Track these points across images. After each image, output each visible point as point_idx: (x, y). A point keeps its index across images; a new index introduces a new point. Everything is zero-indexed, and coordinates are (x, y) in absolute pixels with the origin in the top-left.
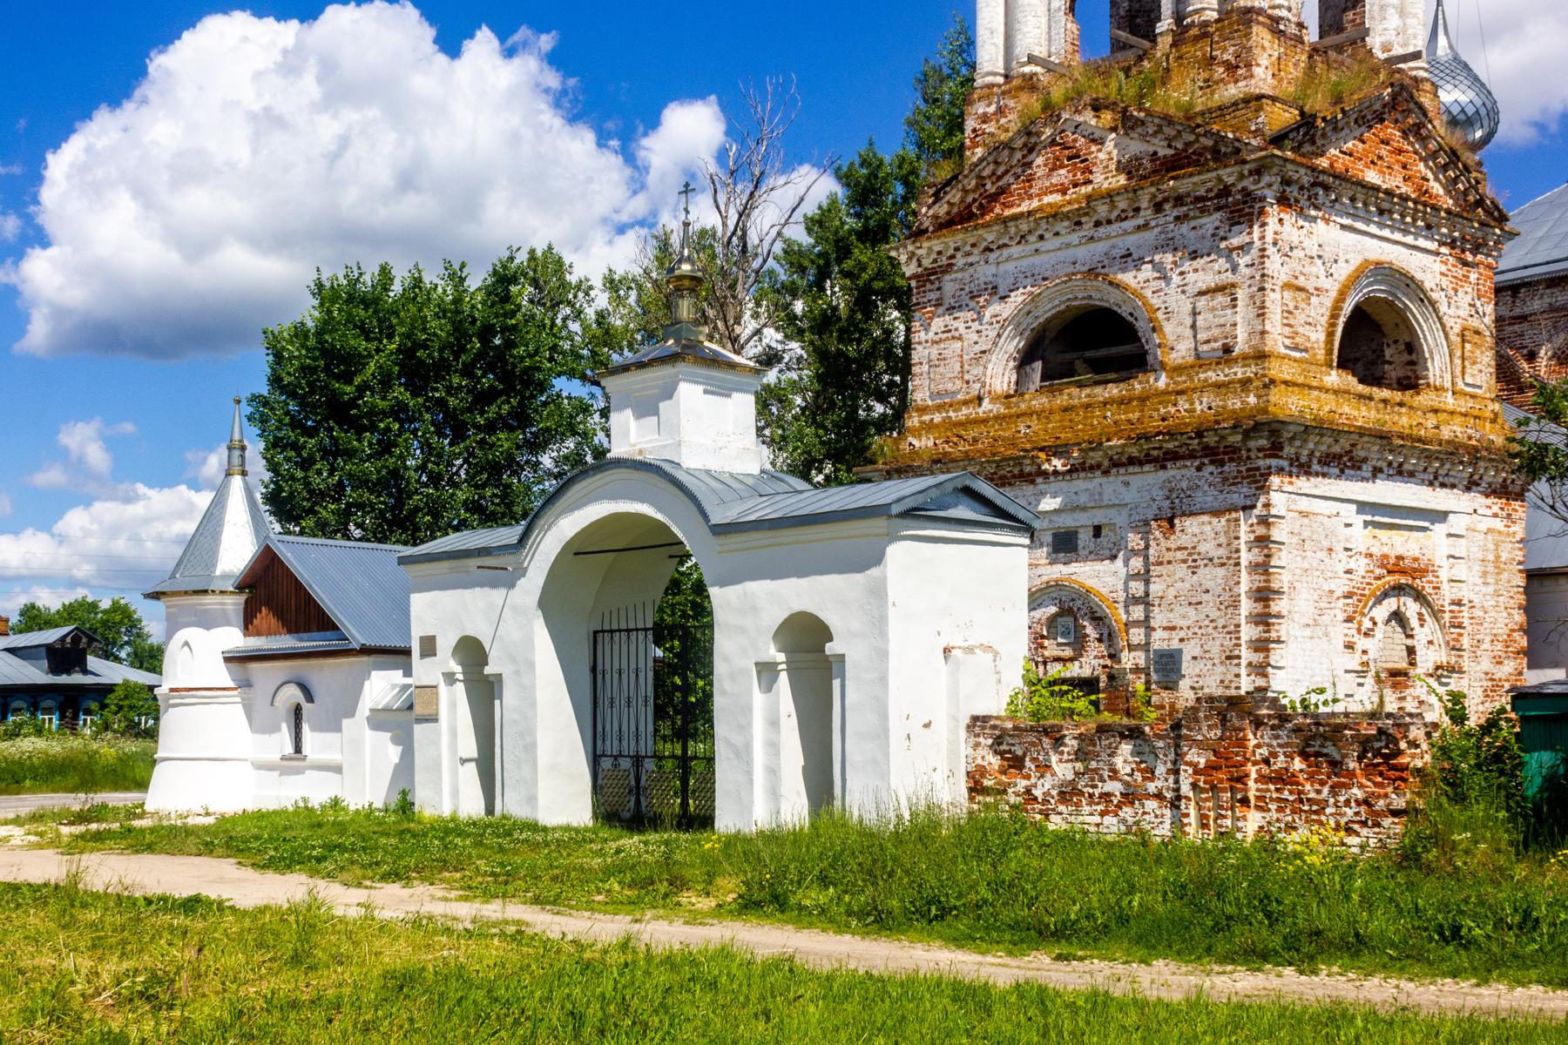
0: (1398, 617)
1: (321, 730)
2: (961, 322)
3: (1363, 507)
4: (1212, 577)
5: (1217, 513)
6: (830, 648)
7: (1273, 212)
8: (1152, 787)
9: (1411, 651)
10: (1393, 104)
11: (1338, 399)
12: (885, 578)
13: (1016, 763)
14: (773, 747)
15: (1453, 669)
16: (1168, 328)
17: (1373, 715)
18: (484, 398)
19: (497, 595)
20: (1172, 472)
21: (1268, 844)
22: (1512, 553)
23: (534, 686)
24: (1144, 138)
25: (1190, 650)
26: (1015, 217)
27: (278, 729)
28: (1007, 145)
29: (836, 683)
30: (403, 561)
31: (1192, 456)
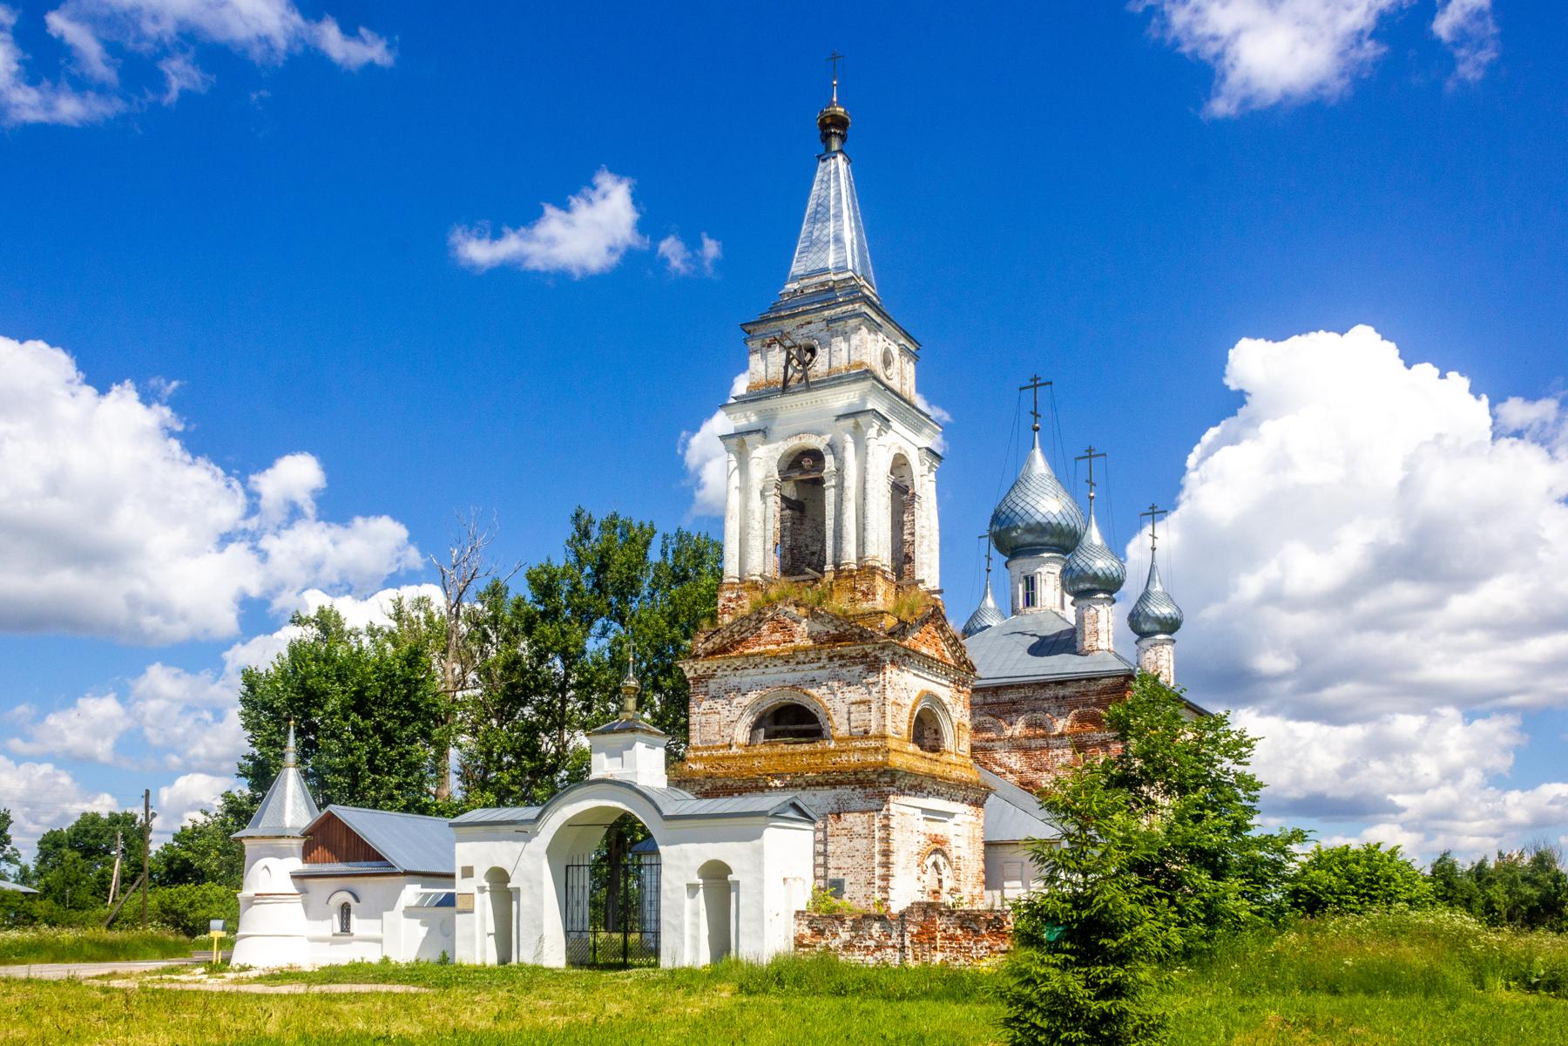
0: (935, 864)
1: (364, 917)
2: (719, 705)
3: (924, 811)
4: (860, 844)
5: (863, 812)
6: (730, 878)
7: (888, 667)
8: (890, 943)
9: (940, 881)
10: (932, 616)
11: (908, 757)
12: (762, 847)
13: (821, 933)
14: (696, 926)
15: (958, 890)
16: (835, 719)
17: (991, 911)
18: (405, 722)
19: (519, 846)
20: (839, 790)
21: (944, 963)
22: (979, 833)
23: (542, 894)
24: (823, 624)
25: (848, 880)
26: (753, 655)
27: (331, 917)
28: (748, 618)
29: (733, 895)
30: (451, 825)
31: (850, 783)
